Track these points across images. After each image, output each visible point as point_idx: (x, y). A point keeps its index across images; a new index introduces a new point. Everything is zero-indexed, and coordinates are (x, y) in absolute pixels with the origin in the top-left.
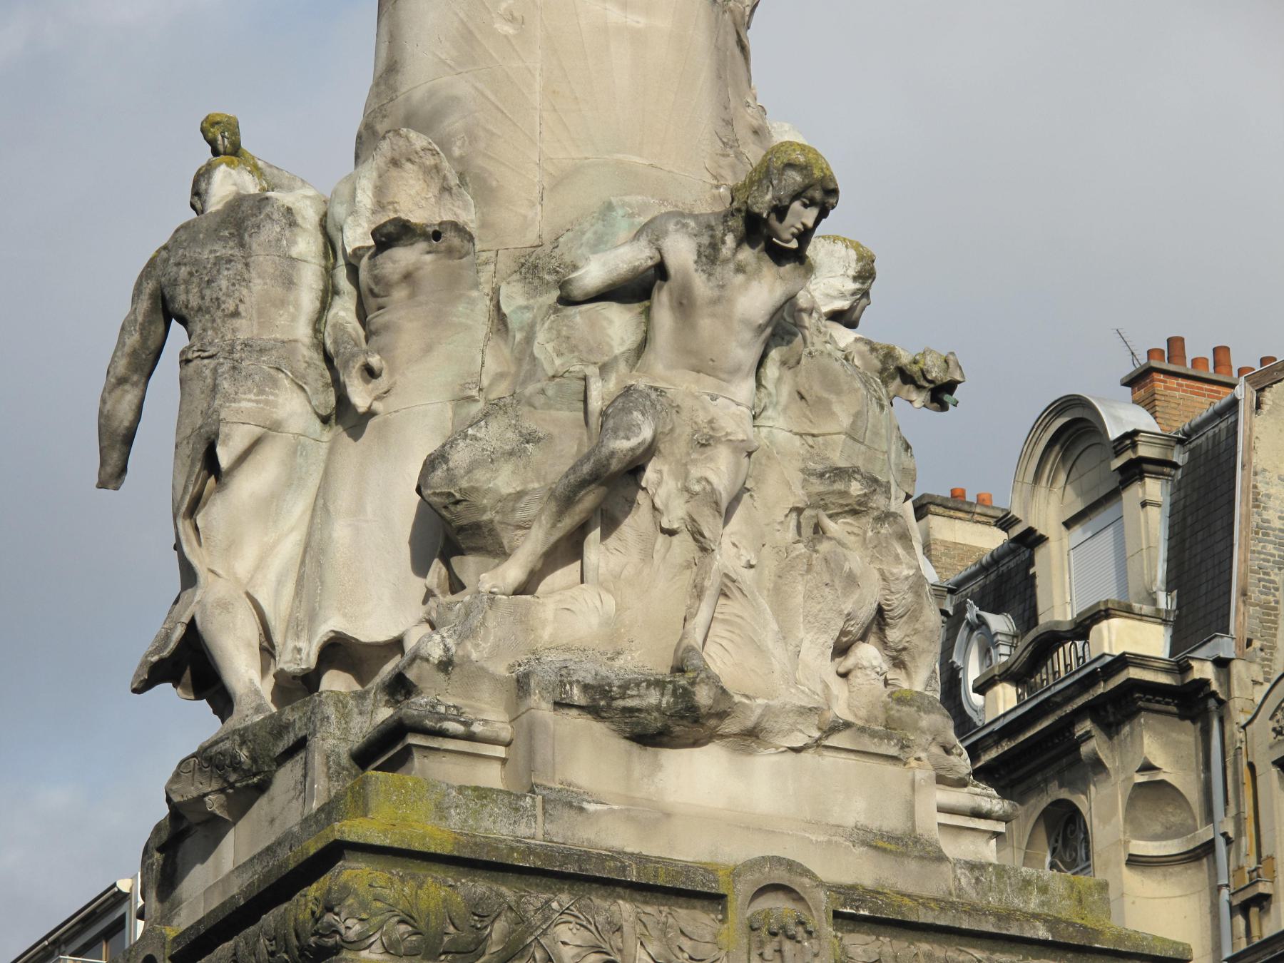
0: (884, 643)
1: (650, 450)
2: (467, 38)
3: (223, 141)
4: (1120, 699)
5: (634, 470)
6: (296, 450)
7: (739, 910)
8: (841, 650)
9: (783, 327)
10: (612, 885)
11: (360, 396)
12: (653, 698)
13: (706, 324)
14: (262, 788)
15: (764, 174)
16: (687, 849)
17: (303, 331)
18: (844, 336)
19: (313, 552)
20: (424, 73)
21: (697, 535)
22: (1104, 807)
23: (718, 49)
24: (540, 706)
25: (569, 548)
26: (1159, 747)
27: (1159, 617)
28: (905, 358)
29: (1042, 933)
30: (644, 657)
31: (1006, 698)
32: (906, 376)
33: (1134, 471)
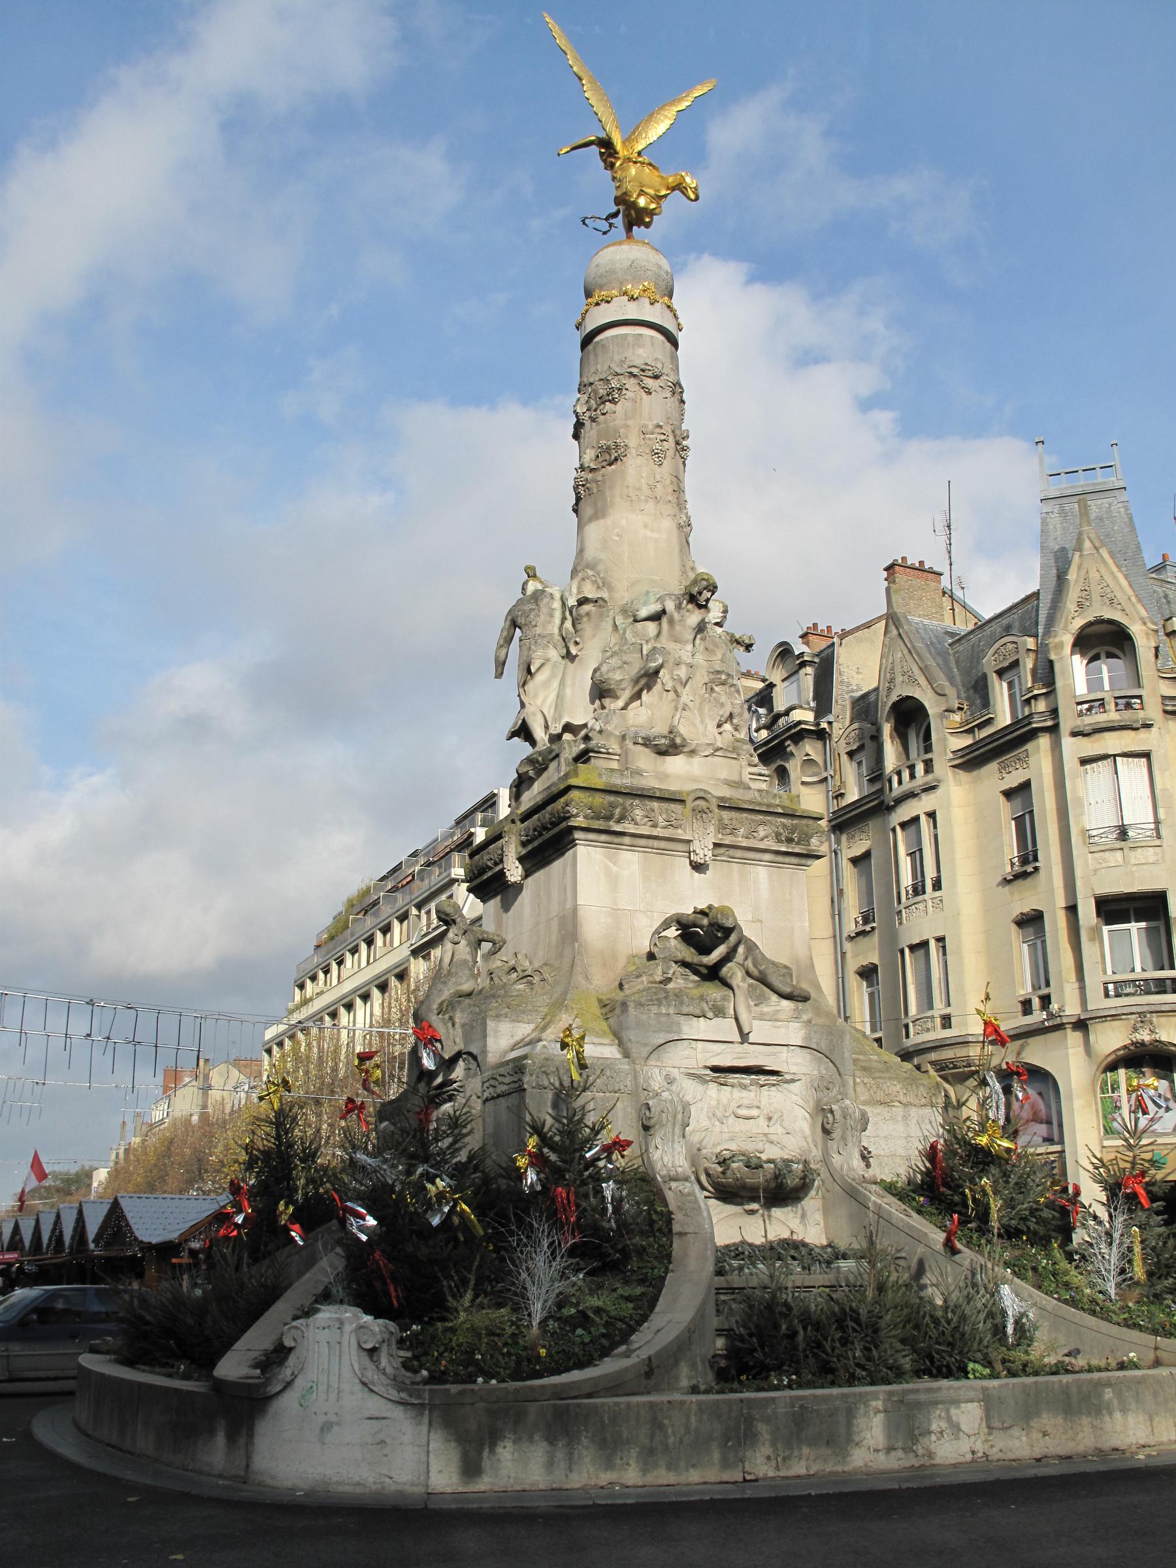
0: (732, 724)
1: (661, 666)
2: (605, 541)
3: (531, 573)
4: (799, 734)
5: (657, 672)
6: (555, 666)
7: (690, 804)
8: (719, 726)
9: (701, 628)
10: (651, 797)
11: (574, 651)
12: (663, 741)
13: (678, 628)
14: (546, 768)
15: (695, 582)
16: (673, 786)
17: (556, 631)
18: (719, 630)
19: (560, 697)
20: (590, 553)
21: (676, 691)
22: (794, 767)
23: (681, 543)
24: (629, 743)
25: (637, 696)
26: (810, 748)
27: (810, 709)
28: (737, 637)
29: (780, 811)
30: (660, 729)
31: (764, 734)
32: (738, 642)
33: (803, 664)
